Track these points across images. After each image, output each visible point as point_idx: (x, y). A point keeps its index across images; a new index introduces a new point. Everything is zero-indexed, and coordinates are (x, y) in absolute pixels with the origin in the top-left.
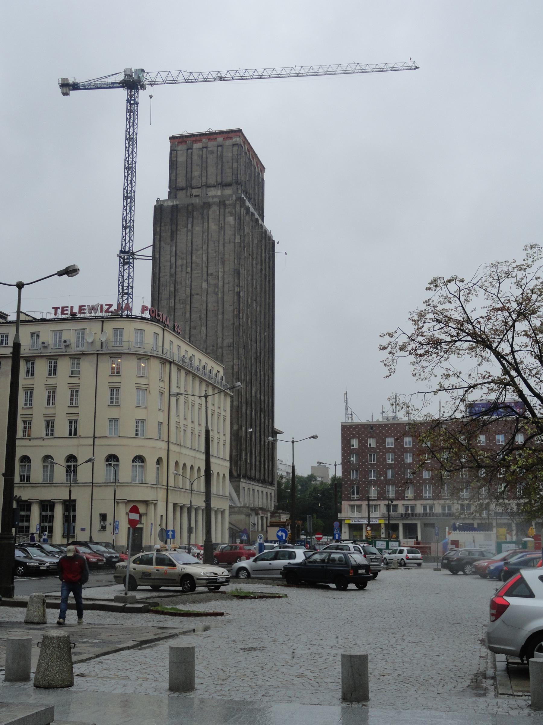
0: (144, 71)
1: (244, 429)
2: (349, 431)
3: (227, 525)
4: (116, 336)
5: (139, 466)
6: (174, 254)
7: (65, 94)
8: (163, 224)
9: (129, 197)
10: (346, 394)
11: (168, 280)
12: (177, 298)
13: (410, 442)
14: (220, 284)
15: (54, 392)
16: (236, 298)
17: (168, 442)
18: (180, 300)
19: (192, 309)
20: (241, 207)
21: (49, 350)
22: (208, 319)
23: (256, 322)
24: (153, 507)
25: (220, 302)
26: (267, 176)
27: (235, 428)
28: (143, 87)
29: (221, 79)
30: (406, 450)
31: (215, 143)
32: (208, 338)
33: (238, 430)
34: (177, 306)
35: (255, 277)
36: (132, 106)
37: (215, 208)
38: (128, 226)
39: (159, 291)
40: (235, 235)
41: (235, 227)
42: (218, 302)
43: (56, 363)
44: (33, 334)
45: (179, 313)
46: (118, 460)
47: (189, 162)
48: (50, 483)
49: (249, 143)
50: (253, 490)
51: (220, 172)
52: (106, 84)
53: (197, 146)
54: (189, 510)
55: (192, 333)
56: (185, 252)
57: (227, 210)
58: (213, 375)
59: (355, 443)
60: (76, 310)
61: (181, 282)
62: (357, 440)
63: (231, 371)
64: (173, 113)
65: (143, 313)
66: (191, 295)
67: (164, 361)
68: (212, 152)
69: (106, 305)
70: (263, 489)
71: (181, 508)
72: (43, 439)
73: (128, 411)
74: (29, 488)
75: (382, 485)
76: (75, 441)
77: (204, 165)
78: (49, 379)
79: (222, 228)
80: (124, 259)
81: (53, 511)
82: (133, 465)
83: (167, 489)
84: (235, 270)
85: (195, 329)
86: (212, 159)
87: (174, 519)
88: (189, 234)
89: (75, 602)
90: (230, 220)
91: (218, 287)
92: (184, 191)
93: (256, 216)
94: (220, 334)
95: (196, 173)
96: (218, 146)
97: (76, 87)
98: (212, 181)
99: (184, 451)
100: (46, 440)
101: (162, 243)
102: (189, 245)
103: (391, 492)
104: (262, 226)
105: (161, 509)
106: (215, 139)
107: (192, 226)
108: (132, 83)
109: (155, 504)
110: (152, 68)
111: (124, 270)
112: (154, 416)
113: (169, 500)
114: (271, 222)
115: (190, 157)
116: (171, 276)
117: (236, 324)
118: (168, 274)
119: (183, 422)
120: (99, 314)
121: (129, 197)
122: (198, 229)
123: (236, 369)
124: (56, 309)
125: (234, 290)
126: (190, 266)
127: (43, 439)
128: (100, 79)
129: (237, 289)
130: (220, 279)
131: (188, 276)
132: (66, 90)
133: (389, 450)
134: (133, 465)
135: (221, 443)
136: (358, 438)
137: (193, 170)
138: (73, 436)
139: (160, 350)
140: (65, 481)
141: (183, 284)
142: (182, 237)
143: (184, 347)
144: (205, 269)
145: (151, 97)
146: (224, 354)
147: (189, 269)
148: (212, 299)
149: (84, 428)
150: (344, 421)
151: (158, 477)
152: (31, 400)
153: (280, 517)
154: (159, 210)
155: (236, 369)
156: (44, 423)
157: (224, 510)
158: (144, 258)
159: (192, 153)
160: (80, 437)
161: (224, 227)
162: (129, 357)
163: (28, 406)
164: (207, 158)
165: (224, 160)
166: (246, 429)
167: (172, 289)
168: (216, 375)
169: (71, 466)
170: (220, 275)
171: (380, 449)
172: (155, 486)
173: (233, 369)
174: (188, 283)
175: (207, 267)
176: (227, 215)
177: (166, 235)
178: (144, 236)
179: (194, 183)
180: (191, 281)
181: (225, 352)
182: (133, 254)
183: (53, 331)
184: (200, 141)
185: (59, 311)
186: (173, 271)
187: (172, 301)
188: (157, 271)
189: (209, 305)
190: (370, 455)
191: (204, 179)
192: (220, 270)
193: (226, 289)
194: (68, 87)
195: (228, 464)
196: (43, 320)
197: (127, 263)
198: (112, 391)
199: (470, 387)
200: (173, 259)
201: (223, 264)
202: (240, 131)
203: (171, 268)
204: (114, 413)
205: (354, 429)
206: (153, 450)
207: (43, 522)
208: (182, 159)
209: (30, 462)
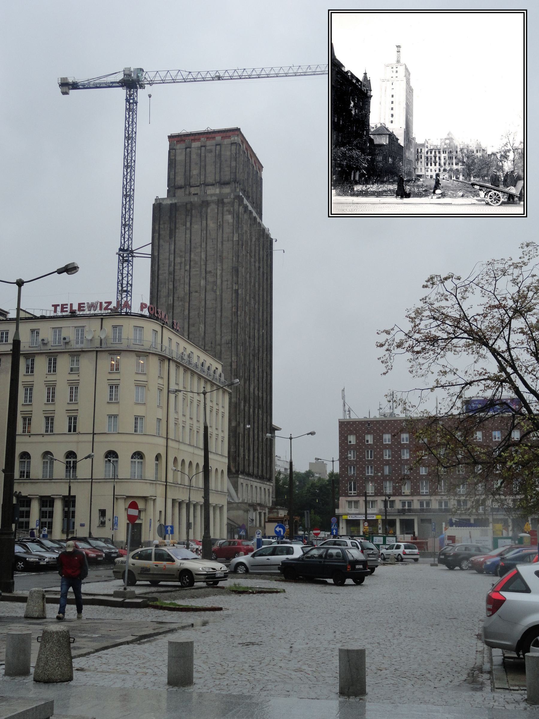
0: (143, 71)
1: (242, 425)
2: (347, 427)
3: (225, 521)
4: (115, 333)
5: (138, 462)
6: (172, 252)
7: (65, 93)
8: (161, 222)
9: (128, 195)
10: (343, 390)
11: (167, 278)
12: (176, 296)
13: (406, 438)
14: (219, 282)
16: (234, 295)
17: (167, 439)
18: (178, 297)
19: (191, 306)
20: (239, 205)
21: (49, 347)
22: (207, 316)
23: (254, 319)
24: (152, 502)
25: (218, 300)
26: (265, 175)
27: (233, 424)
28: (142, 87)
29: (219, 78)
30: (403, 447)
31: (213, 142)
32: (206, 335)
34: (176, 304)
36: (131, 105)
37: (213, 206)
38: (127, 225)
40: (233, 233)
42: (216, 300)
43: (55, 360)
44: (32, 331)
45: (177, 310)
46: (117, 456)
47: (188, 161)
48: (49, 479)
49: (247, 142)
50: (251, 486)
51: (218, 170)
52: (105, 83)
53: (195, 145)
55: (190, 330)
56: (183, 249)
57: (225, 209)
59: (352, 439)
60: (75, 307)
61: (179, 280)
62: (355, 437)
63: (229, 368)
64: (172, 112)
65: (142, 310)
66: (190, 293)
67: (163, 358)
68: (211, 151)
69: (106, 303)
70: (261, 485)
72: (43, 435)
73: (128, 408)
75: (380, 481)
76: (74, 438)
77: (203, 164)
79: (220, 226)
80: (123, 257)
81: (53, 506)
82: (132, 462)
83: (166, 485)
84: (233, 267)
86: (210, 158)
87: (173, 514)
88: (188, 232)
89: (74, 597)
90: (229, 218)
91: (216, 285)
92: (183, 190)
93: (255, 214)
94: (218, 331)
95: (195, 172)
96: (216, 145)
97: (75, 86)
98: (210, 180)
99: (182, 447)
100: (45, 437)
101: (161, 241)
102: (188, 243)
103: (389, 488)
104: (260, 224)
106: (214, 138)
107: (191, 224)
108: (131, 83)
109: (154, 500)
112: (153, 413)
113: (168, 496)
114: (269, 220)
115: (188, 156)
116: (170, 273)
117: (235, 321)
118: (167, 272)
119: (181, 419)
120: (98, 311)
121: (128, 195)
122: (196, 227)
123: (234, 366)
124: (55, 306)
125: (232, 288)
126: (188, 264)
127: (43, 435)
128: (100, 78)
129: (235, 287)
130: (218, 277)
131: (187, 274)
132: (65, 89)
133: (386, 447)
134: (132, 462)
135: (220, 439)
138: (72, 432)
139: (159, 347)
140: (64, 478)
142: (181, 234)
143: (183, 344)
145: (150, 96)
147: (188, 267)
148: (210, 296)
150: (341, 417)
151: (157, 474)
152: (31, 397)
153: (278, 513)
154: (158, 208)
155: (234, 366)
156: (44, 420)
157: (223, 506)
158: (143, 256)
160: (79, 433)
161: (223, 225)
162: (128, 354)
163: (28, 403)
165: (222, 159)
166: (244, 426)
167: (171, 287)
169: (70, 462)
170: (219, 272)
171: (377, 446)
172: (154, 482)
173: (231, 366)
174: (187, 280)
175: (206, 265)
177: (165, 233)
178: (143, 234)
180: (190, 279)
181: (223, 350)
182: (132, 252)
183: (53, 328)
184: (199, 140)
185: (59, 309)
186: (172, 269)
187: (171, 298)
188: (156, 269)
189: (208, 302)
190: (368, 451)
191: (202, 177)
192: (219, 268)
193: (224, 287)
194: (67, 86)
195: (226, 460)
196: (43, 317)
197: (126, 261)
198: (111, 387)
199: (466, 384)
200: (172, 257)
201: (222, 262)
202: (238, 130)
203: (169, 266)
204: (113, 410)
205: (352, 425)
206: (152, 446)
207: (43, 517)
208: (180, 157)
209: (30, 458)
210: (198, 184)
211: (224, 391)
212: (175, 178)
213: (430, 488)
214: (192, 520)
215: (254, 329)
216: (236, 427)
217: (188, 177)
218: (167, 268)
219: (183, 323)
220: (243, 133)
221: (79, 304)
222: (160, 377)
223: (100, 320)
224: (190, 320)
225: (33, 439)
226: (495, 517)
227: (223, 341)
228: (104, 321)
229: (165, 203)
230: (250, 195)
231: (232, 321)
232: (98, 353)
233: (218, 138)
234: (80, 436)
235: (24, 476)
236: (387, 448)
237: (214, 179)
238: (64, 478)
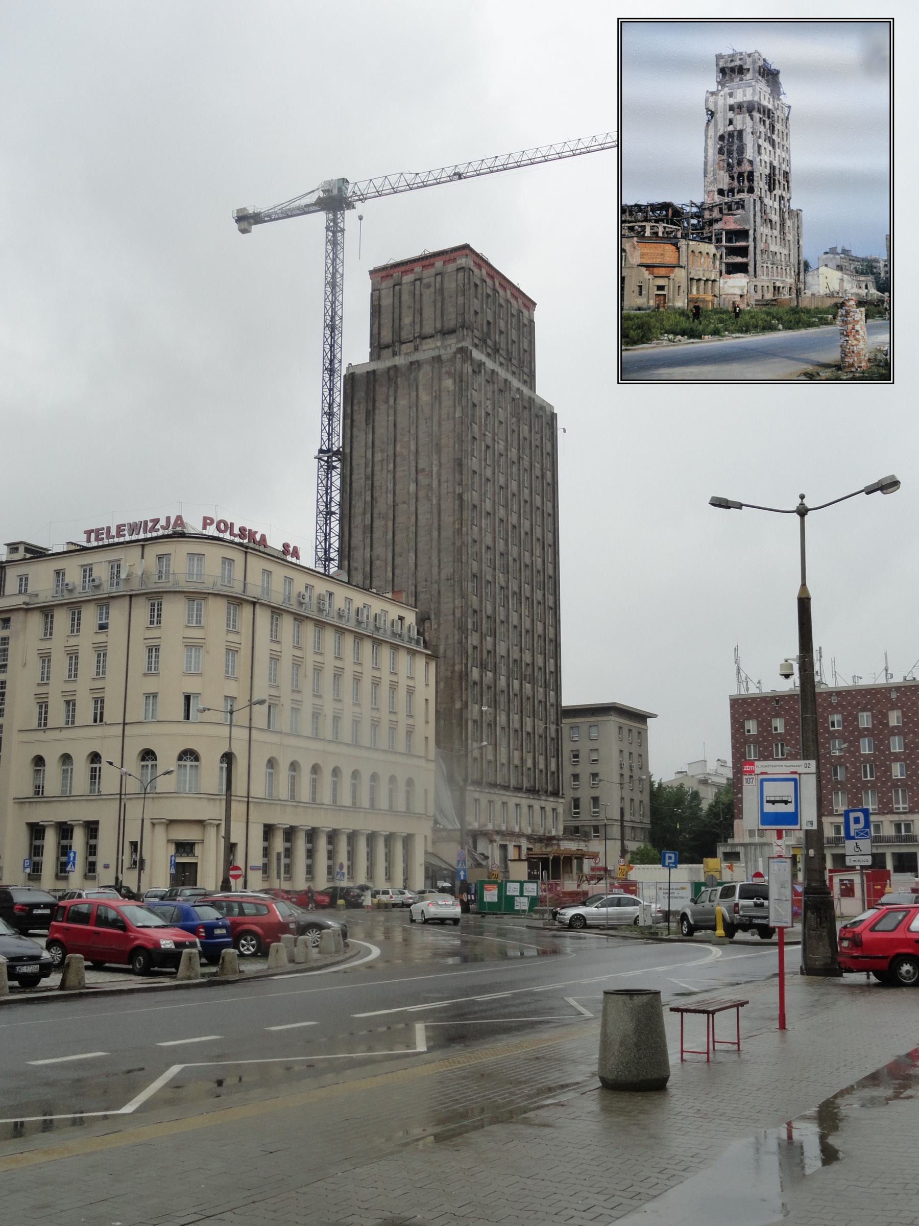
0: (347, 182)
4: (160, 566)
5: (191, 766)
6: (370, 444)
7: (244, 231)
8: (355, 402)
10: (736, 650)
12: (376, 511)
13: (838, 721)
16: (457, 503)
17: (250, 728)
18: (380, 514)
19: (396, 525)
21: (76, 594)
22: (419, 540)
25: (435, 511)
26: (539, 316)
28: (350, 206)
29: (460, 176)
31: (432, 271)
32: (419, 568)
33: (461, 709)
36: (335, 232)
37: (426, 368)
39: (350, 504)
40: (455, 406)
41: (454, 395)
42: (431, 512)
44: (58, 573)
45: (378, 534)
46: (197, 759)
48: (66, 796)
51: (439, 313)
52: (298, 208)
55: (396, 563)
56: (385, 440)
57: (444, 370)
59: (752, 726)
62: (755, 722)
64: (389, 234)
65: (204, 528)
68: (428, 286)
69: (151, 521)
70: (532, 802)
72: (61, 729)
73: (172, 684)
74: (43, 804)
76: (98, 731)
77: (418, 306)
79: (438, 398)
82: (180, 766)
83: (248, 802)
85: (401, 556)
86: (428, 294)
88: (391, 412)
90: (448, 383)
94: (435, 561)
95: (407, 320)
97: (257, 218)
98: (428, 329)
100: (64, 731)
101: (355, 430)
106: (433, 265)
108: (335, 201)
110: (359, 177)
114: (548, 387)
116: (366, 478)
117: (458, 544)
118: (363, 476)
122: (403, 402)
123: (458, 615)
124: (89, 533)
125: (454, 492)
126: (392, 462)
127: (61, 729)
128: (292, 201)
129: (458, 490)
130: (434, 477)
131: (390, 476)
132: (245, 225)
133: (864, 733)
134: (143, 766)
136: (756, 718)
137: (403, 315)
138: (98, 723)
140: (88, 793)
141: (384, 487)
142: (382, 417)
144: (413, 463)
145: (361, 218)
146: (442, 592)
147: (391, 466)
149: (112, 713)
150: (734, 692)
153: (559, 845)
155: (458, 615)
161: (440, 396)
164: (421, 295)
165: (446, 294)
167: (369, 499)
170: (435, 469)
171: (791, 735)
173: (454, 614)
174: (390, 486)
177: (360, 417)
179: (405, 335)
180: (394, 484)
181: (443, 589)
183: (82, 566)
186: (369, 470)
187: (368, 516)
188: (348, 473)
189: (420, 517)
190: (777, 745)
191: (417, 327)
192: (435, 462)
193: (444, 491)
194: (246, 220)
198: (150, 651)
201: (439, 452)
202: (466, 247)
203: (366, 467)
204: (151, 685)
208: (386, 302)
211: (412, 653)
213: (880, 802)
217: (397, 329)
218: (363, 471)
219: (386, 552)
220: (478, 251)
223: (140, 549)
224: (396, 547)
225: (51, 735)
227: (443, 575)
228: (147, 549)
231: (454, 544)
232: (133, 599)
233: (418, 269)
234: (107, 727)
236: (865, 736)
237: (446, 330)
238: (88, 793)
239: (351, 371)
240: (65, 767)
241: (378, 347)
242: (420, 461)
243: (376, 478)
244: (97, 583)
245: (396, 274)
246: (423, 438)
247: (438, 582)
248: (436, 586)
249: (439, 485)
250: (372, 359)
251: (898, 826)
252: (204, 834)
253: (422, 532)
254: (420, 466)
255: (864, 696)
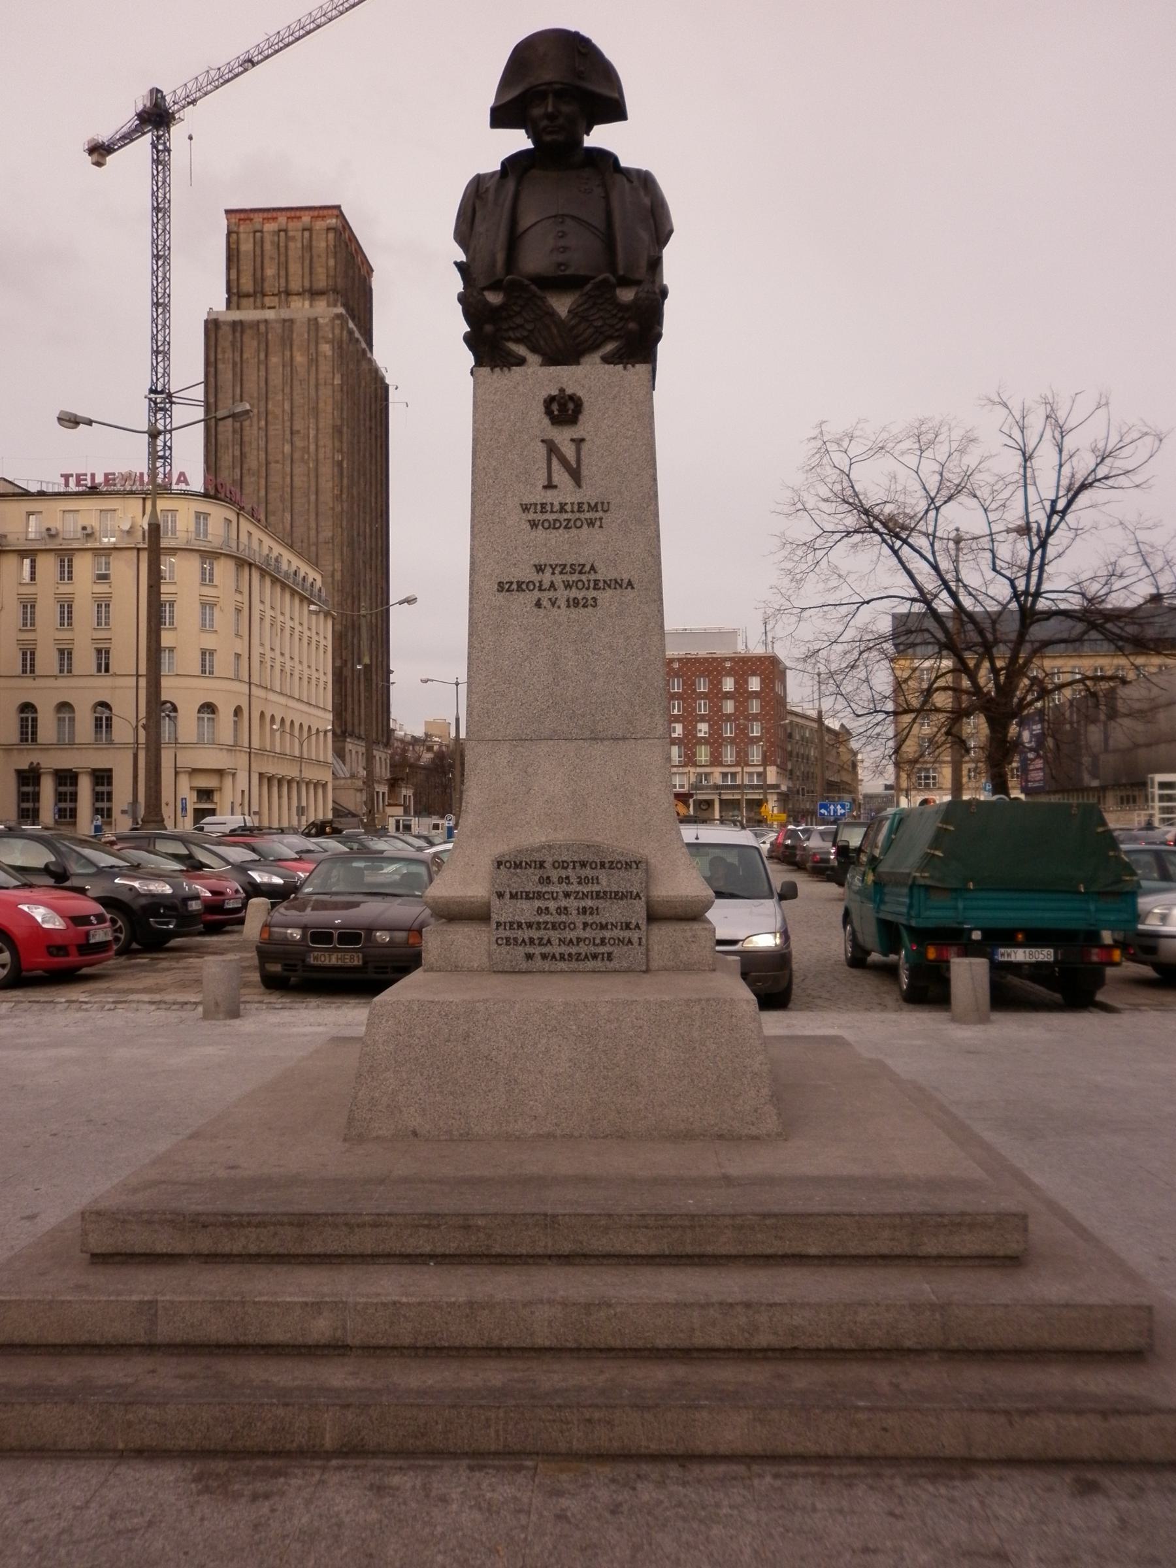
1: (349, 665)
3: (330, 805)
9: (161, 304)
11: (230, 438)
12: (246, 466)
15: (70, 607)
17: (250, 684)
20: (342, 329)
23: (364, 507)
24: (230, 778)
25: (312, 475)
27: (338, 664)
34: (246, 480)
35: (362, 439)
38: (160, 352)
43: (70, 561)
47: (258, 252)
48: (67, 743)
49: (350, 228)
51: (307, 270)
53: (270, 227)
54: (280, 781)
56: (255, 395)
58: (308, 584)
60: (99, 479)
61: (250, 443)
63: (330, 580)
66: (267, 463)
67: (242, 563)
71: (270, 779)
72: (56, 677)
76: (106, 681)
78: (61, 587)
79: (313, 361)
80: (156, 403)
81: (76, 784)
86: (295, 248)
87: (260, 795)
88: (262, 367)
91: (308, 453)
92: (252, 299)
93: (364, 345)
94: (313, 525)
95: (270, 272)
99: (273, 697)
102: (263, 384)
104: (370, 361)
105: (242, 777)
107: (266, 356)
109: (234, 775)
111: (156, 421)
112: (225, 644)
113: (253, 768)
115: (259, 243)
119: (269, 654)
121: (161, 304)
124: (67, 477)
127: (56, 677)
131: (262, 433)
133: (728, 696)
135: (322, 685)
136: (759, 675)
139: (234, 545)
141: (254, 445)
143: (268, 542)
144: (288, 424)
145: (190, 138)
147: (263, 423)
148: (299, 469)
151: (236, 736)
152: (33, 619)
154: (212, 327)
156: (56, 655)
158: (191, 402)
159: (262, 238)
160: (115, 675)
162: (187, 554)
163: (29, 627)
166: (353, 666)
167: (237, 453)
168: (312, 585)
169: (27, 719)
170: (312, 433)
172: (232, 748)
173: (333, 576)
174: (262, 444)
175: (292, 420)
176: (321, 341)
178: (188, 368)
180: (267, 442)
182: (170, 395)
184: (275, 219)
185: (72, 481)
187: (238, 471)
189: (296, 479)
191: (283, 281)
193: (321, 456)
195: (330, 716)
196: (41, 494)
197: (161, 409)
199: (863, 603)
202: (338, 207)
205: (753, 664)
206: (226, 694)
207: (23, 801)
208: (246, 247)
209: (36, 711)
210: (276, 292)
212: (238, 279)
214: (304, 804)
215: (364, 521)
216: (341, 668)
217: (259, 279)
221: (106, 475)
222: (238, 591)
223: (141, 501)
225: (40, 683)
226: (724, 797)
229: (221, 318)
230: (356, 313)
233: (282, 220)
234: (75, 679)
235: (27, 740)
239: (214, 317)
240: (61, 715)
241: (235, 295)
242: (295, 422)
243: (245, 433)
244: (89, 531)
245: (258, 218)
246: (298, 400)
247: (317, 544)
248: (313, 548)
249: (317, 450)
250: (228, 307)
251: (724, 775)
252: (221, 782)
253: (297, 494)
254: (296, 428)
255: (693, 664)
